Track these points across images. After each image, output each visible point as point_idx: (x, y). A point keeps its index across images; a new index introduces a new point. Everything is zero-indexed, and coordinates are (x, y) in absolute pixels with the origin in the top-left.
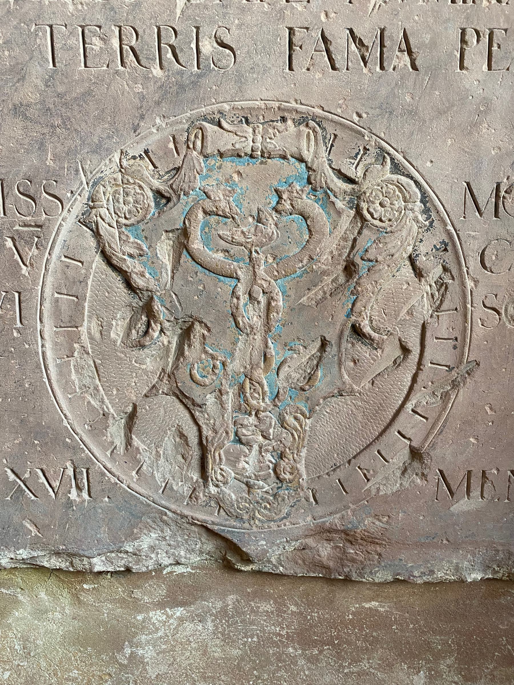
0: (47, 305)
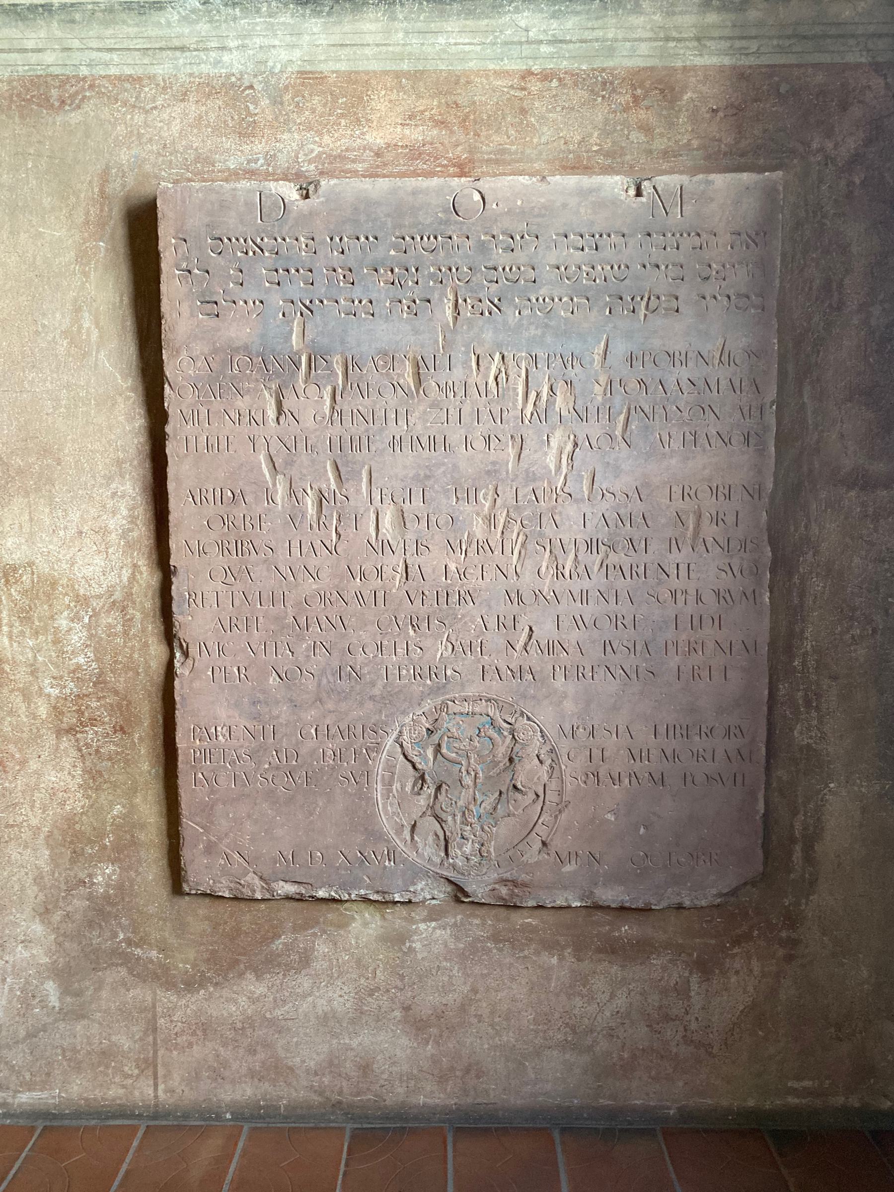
0: (379, 777)
